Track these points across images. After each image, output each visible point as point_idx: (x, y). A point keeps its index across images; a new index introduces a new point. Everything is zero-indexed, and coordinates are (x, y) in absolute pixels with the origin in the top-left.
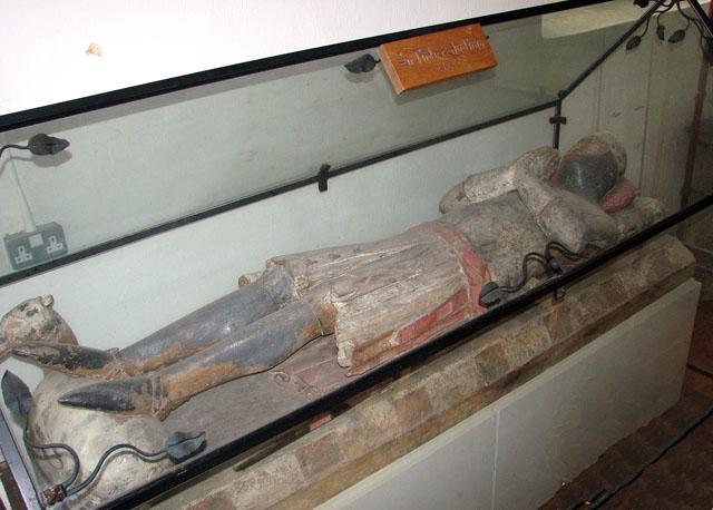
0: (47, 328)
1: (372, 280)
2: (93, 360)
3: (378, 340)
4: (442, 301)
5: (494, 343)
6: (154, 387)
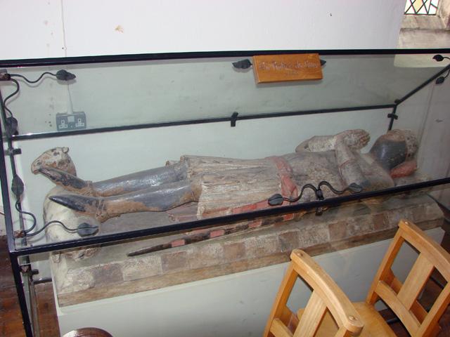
0: (61, 163)
1: (226, 179)
2: (79, 184)
3: (219, 210)
4: (263, 199)
5: (293, 230)
6: (100, 204)
